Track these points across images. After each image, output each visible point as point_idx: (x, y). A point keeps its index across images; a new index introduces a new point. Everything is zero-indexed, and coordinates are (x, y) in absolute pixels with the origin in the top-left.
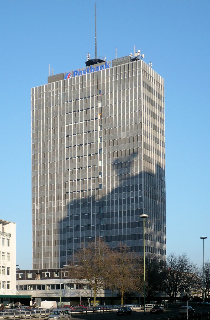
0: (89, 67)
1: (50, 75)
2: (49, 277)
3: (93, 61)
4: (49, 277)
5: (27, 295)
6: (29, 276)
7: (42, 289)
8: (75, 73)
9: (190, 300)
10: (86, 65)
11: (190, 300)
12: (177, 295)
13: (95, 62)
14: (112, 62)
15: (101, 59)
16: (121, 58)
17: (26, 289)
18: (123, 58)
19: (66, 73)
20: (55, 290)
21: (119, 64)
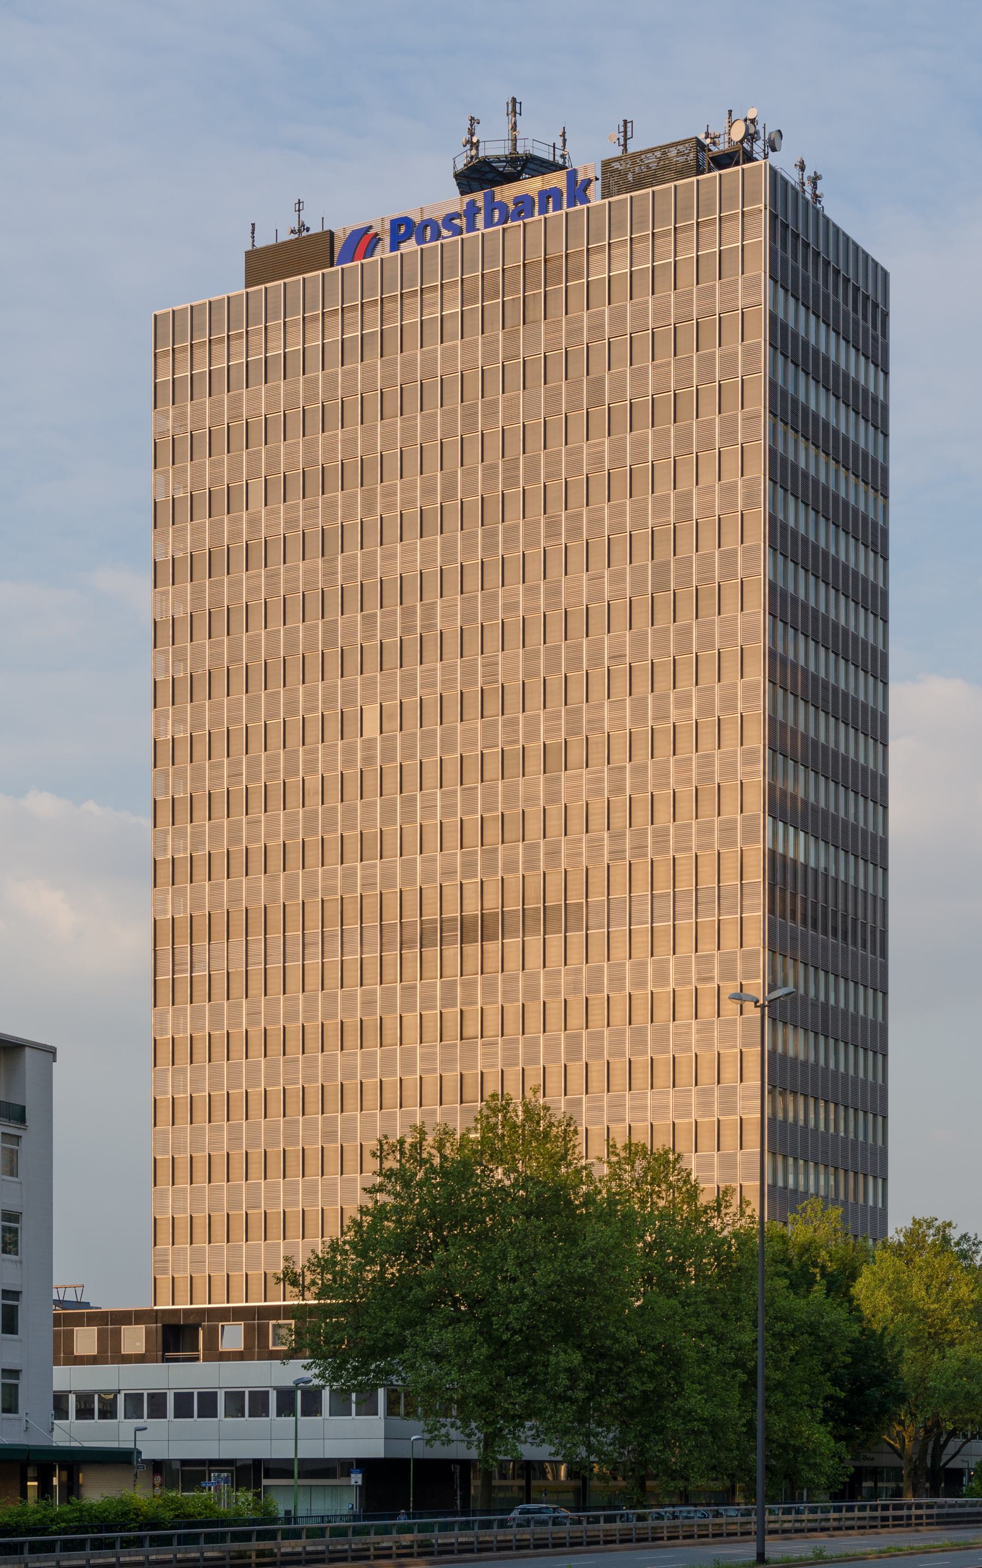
0: (479, 197)
1: (250, 248)
2: (271, 1348)
3: (500, 166)
4: (271, 1348)
5: (114, 1445)
6: (134, 1339)
7: (18, 1379)
8: (403, 229)
9: (126, 1350)
10: (456, 190)
11: (126, 1350)
12: (944, 1458)
13: (509, 169)
14: (603, 173)
15: (544, 153)
16: (652, 151)
17: (108, 1412)
18: (664, 148)
19: (348, 232)
20: (274, 1421)
21: (639, 184)
